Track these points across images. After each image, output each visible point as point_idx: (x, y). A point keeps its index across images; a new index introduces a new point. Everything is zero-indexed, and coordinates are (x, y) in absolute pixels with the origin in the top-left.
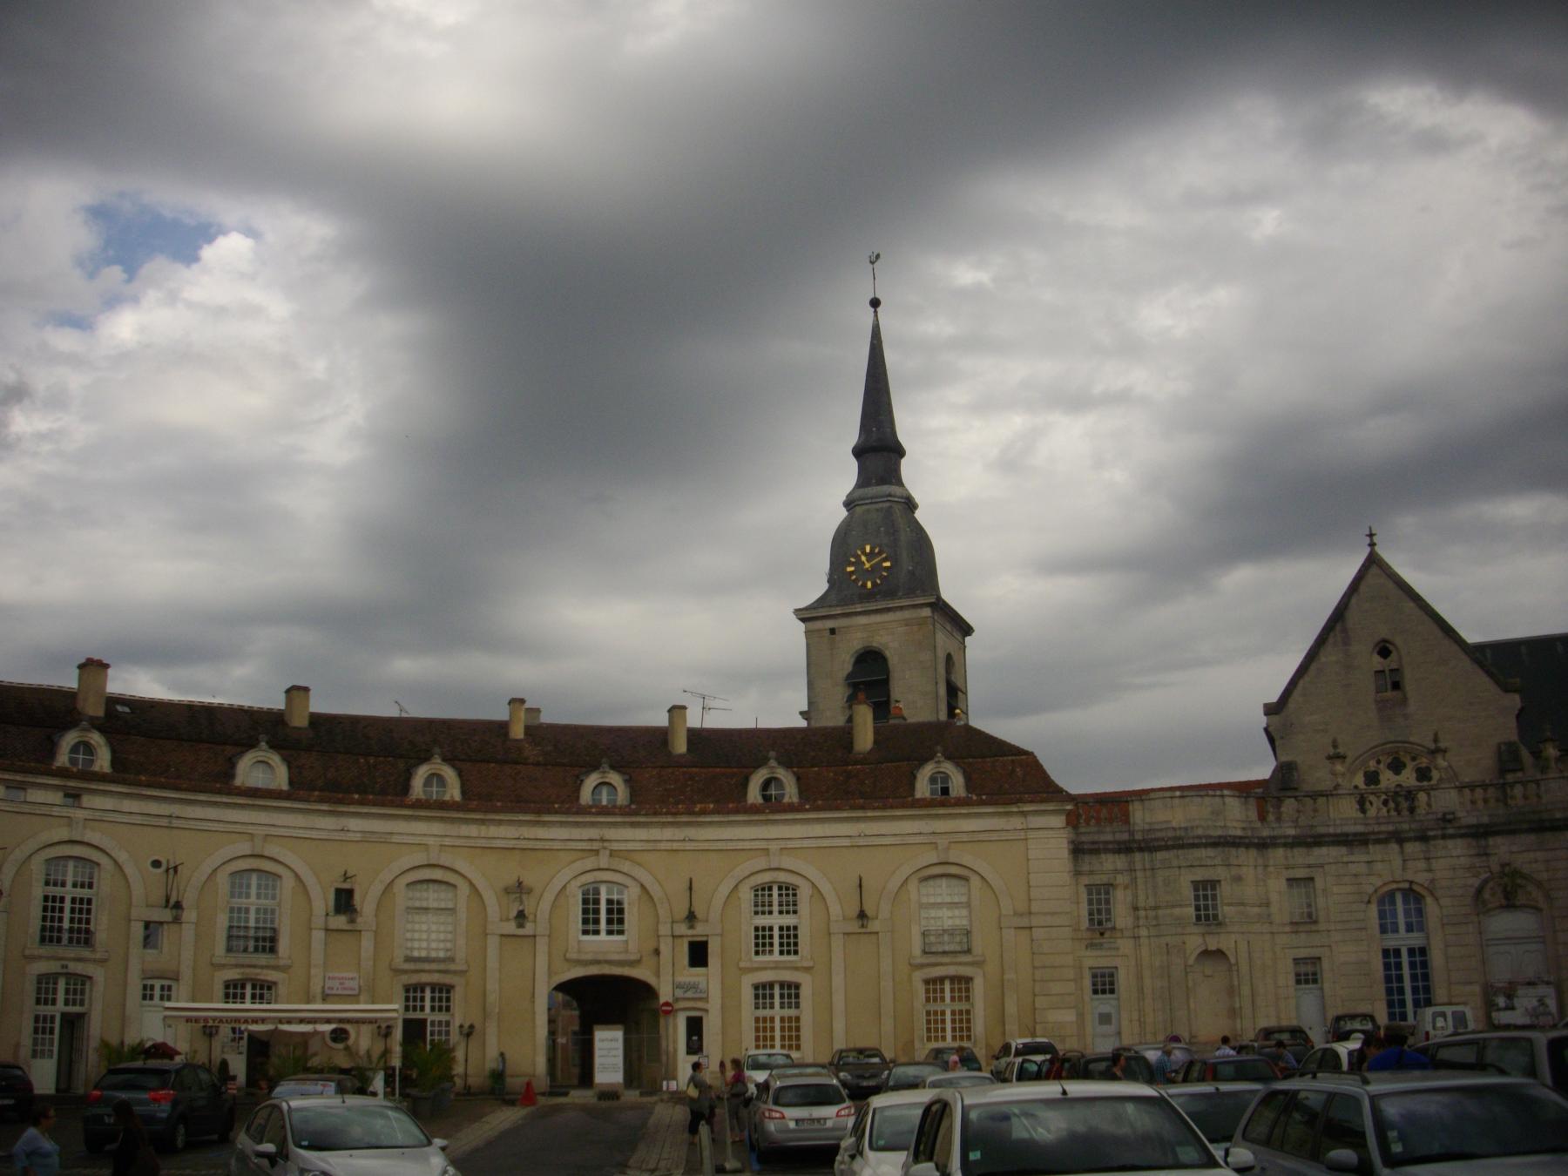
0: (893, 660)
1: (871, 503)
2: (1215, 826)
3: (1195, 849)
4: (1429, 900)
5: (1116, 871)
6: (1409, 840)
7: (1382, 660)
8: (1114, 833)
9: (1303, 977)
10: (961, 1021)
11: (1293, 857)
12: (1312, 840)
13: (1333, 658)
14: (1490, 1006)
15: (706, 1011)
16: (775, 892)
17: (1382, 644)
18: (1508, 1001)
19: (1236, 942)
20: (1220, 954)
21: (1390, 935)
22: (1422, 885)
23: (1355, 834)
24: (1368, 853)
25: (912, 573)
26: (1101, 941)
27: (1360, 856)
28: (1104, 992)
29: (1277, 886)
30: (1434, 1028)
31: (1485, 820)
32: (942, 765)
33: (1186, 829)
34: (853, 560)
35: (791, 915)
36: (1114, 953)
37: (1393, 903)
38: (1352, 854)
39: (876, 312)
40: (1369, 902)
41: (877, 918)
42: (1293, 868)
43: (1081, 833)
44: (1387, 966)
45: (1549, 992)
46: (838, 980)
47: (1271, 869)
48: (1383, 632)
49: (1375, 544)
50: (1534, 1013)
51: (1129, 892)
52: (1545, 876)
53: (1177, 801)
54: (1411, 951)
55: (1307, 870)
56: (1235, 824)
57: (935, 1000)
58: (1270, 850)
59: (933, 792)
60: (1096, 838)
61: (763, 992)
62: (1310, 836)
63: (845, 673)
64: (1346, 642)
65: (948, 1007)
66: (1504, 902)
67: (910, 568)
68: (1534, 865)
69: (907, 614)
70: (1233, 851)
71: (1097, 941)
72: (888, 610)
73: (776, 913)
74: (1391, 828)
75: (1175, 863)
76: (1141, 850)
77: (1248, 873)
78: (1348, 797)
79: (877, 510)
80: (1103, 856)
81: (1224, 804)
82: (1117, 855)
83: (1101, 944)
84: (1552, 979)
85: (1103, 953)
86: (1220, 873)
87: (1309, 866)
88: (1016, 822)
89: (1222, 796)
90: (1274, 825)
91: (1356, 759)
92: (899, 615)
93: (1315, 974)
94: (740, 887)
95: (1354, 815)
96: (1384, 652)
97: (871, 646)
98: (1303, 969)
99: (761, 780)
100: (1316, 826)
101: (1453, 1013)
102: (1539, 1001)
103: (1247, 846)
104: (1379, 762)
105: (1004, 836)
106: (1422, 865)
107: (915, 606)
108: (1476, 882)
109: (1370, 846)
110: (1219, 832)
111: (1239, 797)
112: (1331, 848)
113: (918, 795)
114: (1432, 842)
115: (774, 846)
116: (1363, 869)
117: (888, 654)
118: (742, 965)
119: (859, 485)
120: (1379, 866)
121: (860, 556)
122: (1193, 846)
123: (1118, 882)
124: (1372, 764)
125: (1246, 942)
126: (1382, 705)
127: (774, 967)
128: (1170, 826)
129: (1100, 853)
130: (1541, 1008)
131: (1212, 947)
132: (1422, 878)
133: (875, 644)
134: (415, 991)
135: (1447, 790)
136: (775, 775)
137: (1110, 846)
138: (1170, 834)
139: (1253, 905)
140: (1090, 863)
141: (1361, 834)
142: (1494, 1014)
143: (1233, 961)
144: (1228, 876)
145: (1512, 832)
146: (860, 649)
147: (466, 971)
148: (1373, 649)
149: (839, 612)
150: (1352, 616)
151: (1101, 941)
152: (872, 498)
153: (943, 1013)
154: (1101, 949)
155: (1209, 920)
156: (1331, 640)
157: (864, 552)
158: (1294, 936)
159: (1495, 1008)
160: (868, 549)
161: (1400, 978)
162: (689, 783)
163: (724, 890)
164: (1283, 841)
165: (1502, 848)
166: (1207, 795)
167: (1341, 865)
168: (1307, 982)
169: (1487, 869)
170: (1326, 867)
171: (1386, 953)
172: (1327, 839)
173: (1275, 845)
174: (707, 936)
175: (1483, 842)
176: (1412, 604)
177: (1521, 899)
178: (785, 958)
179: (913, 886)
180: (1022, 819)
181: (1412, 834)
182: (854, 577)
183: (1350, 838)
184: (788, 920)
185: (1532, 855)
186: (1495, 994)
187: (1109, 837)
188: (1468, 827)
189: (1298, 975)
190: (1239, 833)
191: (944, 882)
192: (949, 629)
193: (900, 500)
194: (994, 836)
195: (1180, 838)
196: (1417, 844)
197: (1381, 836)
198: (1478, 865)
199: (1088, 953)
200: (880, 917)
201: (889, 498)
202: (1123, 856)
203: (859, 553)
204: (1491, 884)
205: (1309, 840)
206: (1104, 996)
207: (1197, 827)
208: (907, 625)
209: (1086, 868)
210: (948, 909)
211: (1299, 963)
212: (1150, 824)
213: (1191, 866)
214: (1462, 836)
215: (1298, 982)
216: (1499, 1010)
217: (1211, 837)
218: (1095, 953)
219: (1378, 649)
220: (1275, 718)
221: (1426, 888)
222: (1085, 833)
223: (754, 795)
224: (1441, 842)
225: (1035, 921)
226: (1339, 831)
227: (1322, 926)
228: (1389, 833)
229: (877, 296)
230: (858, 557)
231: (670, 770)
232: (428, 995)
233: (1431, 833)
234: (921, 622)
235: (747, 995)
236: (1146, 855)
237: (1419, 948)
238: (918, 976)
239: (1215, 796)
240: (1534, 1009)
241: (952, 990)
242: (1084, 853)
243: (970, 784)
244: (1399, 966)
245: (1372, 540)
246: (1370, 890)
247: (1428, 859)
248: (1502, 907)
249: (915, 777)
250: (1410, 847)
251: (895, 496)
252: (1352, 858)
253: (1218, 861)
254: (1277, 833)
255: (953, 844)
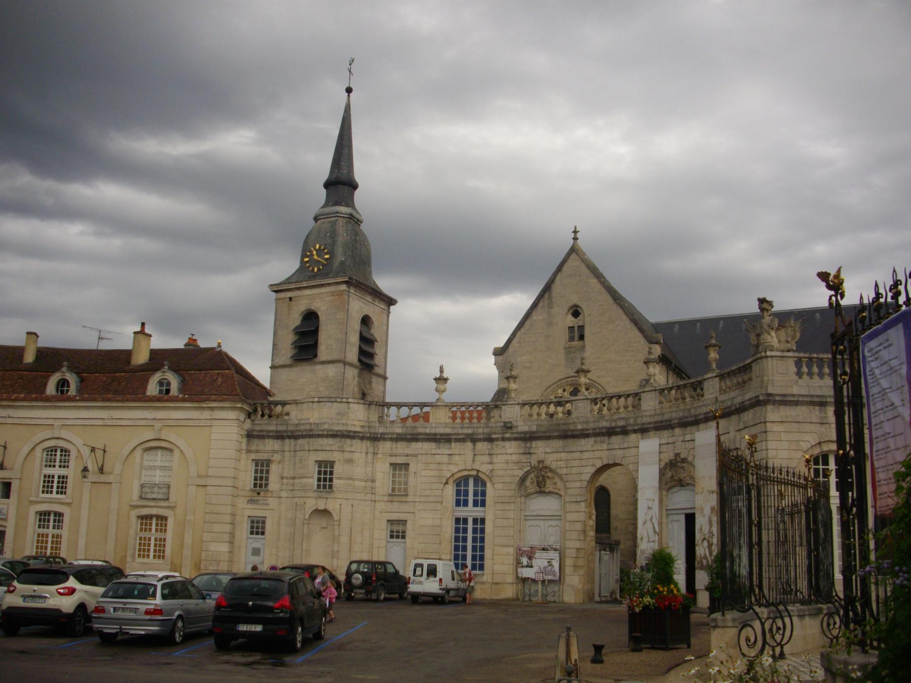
1: (327, 218)
2: (338, 424)
4: (489, 485)
5: (274, 452)
6: (479, 440)
7: (574, 319)
10: (145, 544)
11: (397, 448)
13: (541, 317)
14: (518, 563)
15: (5, 527)
16: (59, 453)
17: (573, 309)
19: (341, 505)
20: (325, 512)
21: (462, 508)
22: (485, 474)
23: (442, 435)
27: (444, 449)
28: (257, 533)
29: (382, 470)
31: (534, 428)
32: (166, 374)
34: (308, 254)
35: (66, 469)
36: (266, 507)
37: (467, 485)
39: (349, 96)
40: (447, 483)
41: (112, 473)
42: (396, 456)
44: (457, 530)
46: (84, 513)
47: (380, 456)
48: (575, 300)
49: (577, 239)
50: (543, 571)
51: (280, 466)
52: (564, 471)
54: (475, 521)
55: (406, 458)
56: (355, 423)
57: (146, 530)
59: (161, 391)
61: (43, 517)
63: (295, 326)
64: (550, 306)
65: (153, 535)
66: (538, 489)
67: (343, 259)
68: (559, 463)
70: (348, 441)
71: (255, 498)
72: (322, 285)
73: (57, 467)
74: (470, 431)
78: (444, 407)
79: (329, 222)
80: (267, 440)
81: (349, 408)
82: (275, 441)
83: (258, 501)
84: (558, 547)
85: (258, 507)
86: (335, 456)
87: (407, 456)
88: (206, 414)
89: (348, 403)
90: (388, 425)
92: (323, 290)
93: (404, 532)
94: (36, 448)
96: (576, 314)
98: (395, 528)
99: (56, 381)
100: (418, 427)
101: (429, 565)
103: (362, 438)
104: (564, 390)
105: (197, 423)
106: (486, 459)
107: (337, 283)
108: (521, 473)
109: (453, 444)
110: (341, 428)
111: (364, 404)
113: (148, 393)
114: (496, 443)
115: (57, 423)
116: (445, 459)
117: (320, 314)
118: (31, 499)
119: (326, 205)
120: (456, 458)
122: (319, 436)
123: (274, 459)
124: (560, 391)
125: (350, 506)
126: (568, 350)
127: (52, 502)
128: (309, 422)
130: (550, 568)
132: (485, 468)
133: (313, 308)
134: (45, 516)
135: (513, 406)
137: (271, 434)
138: (308, 427)
139: (361, 480)
140: (257, 445)
142: (519, 570)
143: (336, 518)
144: (342, 458)
145: (548, 438)
146: (305, 311)
147: (72, 503)
148: (569, 310)
149: (294, 287)
150: (556, 289)
151: (259, 498)
152: (327, 214)
153: (150, 539)
156: (540, 304)
157: (315, 249)
159: (521, 565)
161: (465, 539)
162: (19, 381)
163: (26, 450)
164: (390, 436)
165: (540, 449)
168: (397, 537)
170: (419, 456)
171: (457, 520)
172: (421, 437)
173: (385, 439)
174: (11, 479)
175: (528, 445)
176: (595, 280)
177: (549, 487)
178: (60, 496)
179: (138, 452)
180: (210, 413)
181: (481, 436)
182: (308, 265)
183: (438, 437)
184: (63, 472)
185: (559, 455)
186: (521, 555)
187: (273, 428)
188: (521, 433)
189: (392, 532)
190: (358, 429)
191: (159, 452)
192: (371, 301)
193: (345, 216)
194: (191, 423)
195: (311, 430)
197: (461, 437)
200: (114, 473)
201: (338, 215)
204: (532, 475)
205: (408, 437)
206: (257, 536)
207: (325, 423)
208: (332, 295)
209: (254, 448)
210: (161, 470)
211: (394, 524)
212: (299, 420)
214: (516, 439)
216: (522, 567)
218: (252, 506)
219: (571, 311)
220: (500, 358)
222: (257, 424)
223: (51, 388)
224: (500, 443)
225: (209, 482)
226: (433, 431)
227: (410, 498)
228: (466, 434)
229: (351, 86)
230: (311, 252)
231: (11, 373)
232: (52, 518)
233: (494, 436)
234: (341, 293)
235: (32, 519)
236: (292, 440)
238: (134, 513)
239: (341, 402)
240: (545, 568)
241: (157, 524)
243: (181, 390)
244: (465, 530)
245: (575, 235)
246: (448, 475)
247: (490, 455)
248: (536, 492)
249: (147, 382)
250: (480, 446)
251: (341, 213)
252: (438, 451)
254: (388, 431)
255: (165, 427)
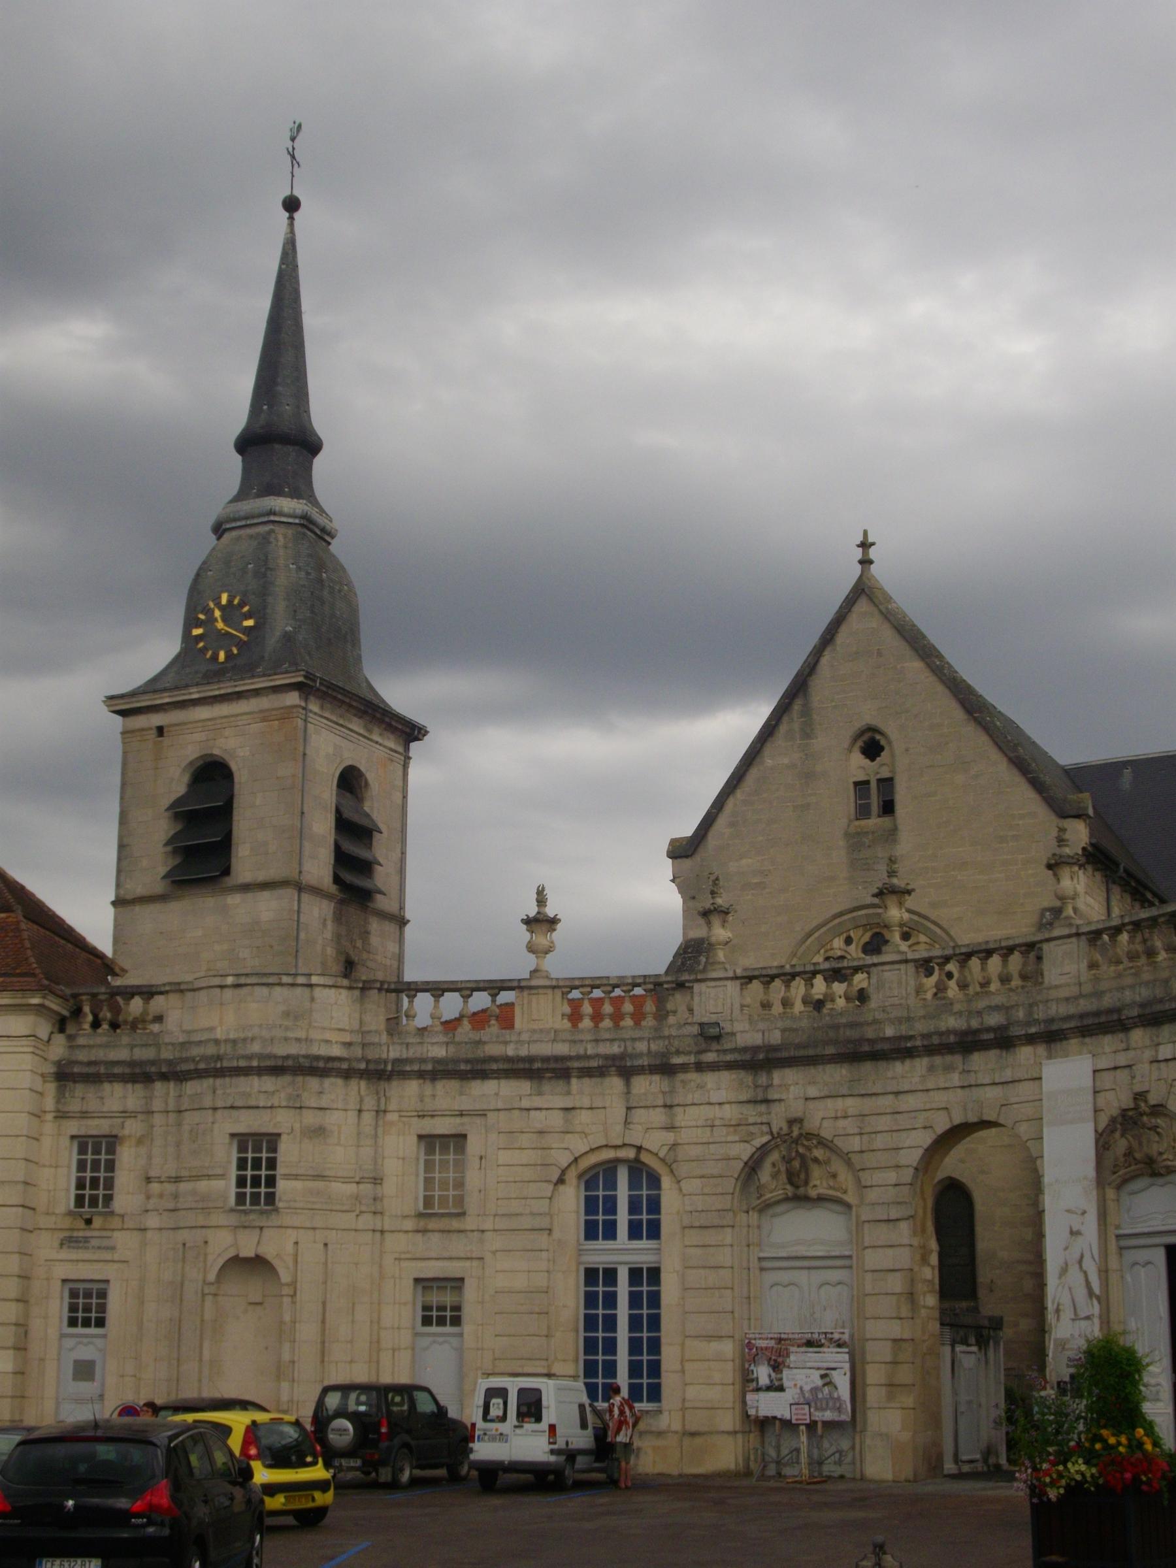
0: (241, 776)
2: (286, 1039)
3: (242, 1079)
4: (666, 1182)
5: (126, 1114)
6: (640, 1070)
8: (132, 1047)
9: (434, 1313)
11: (434, 1096)
12: (469, 1067)
17: (866, 737)
18: (773, 1375)
20: (258, 1264)
21: (601, 1244)
24: (569, 1093)
25: (288, 638)
26: (88, 1234)
27: (553, 1096)
28: (86, 1323)
30: (486, 1417)
31: (776, 1038)
33: (234, 1042)
34: (202, 617)
36: (107, 1256)
37: (612, 1184)
38: (540, 1094)
39: (291, 218)
40: (561, 1181)
42: (433, 1116)
43: (79, 1046)
44: (590, 1300)
45: (838, 1358)
47: (392, 1117)
48: (868, 715)
50: (810, 1400)
51: (143, 1150)
52: (855, 1143)
53: (228, 994)
54: (635, 1274)
55: (458, 1120)
56: (328, 1036)
58: (395, 1083)
60: (100, 1054)
62: (467, 1061)
64: (807, 733)
67: (289, 628)
68: (841, 1123)
69: (264, 702)
70: (313, 1083)
71: (81, 1234)
72: (239, 696)
74: (615, 1049)
75: (207, 1102)
76: (164, 1077)
77: (341, 1122)
78: (550, 991)
79: (251, 537)
81: (312, 999)
82: (129, 1086)
83: (86, 1239)
84: (846, 1337)
85: (87, 1255)
86: (281, 1121)
89: (310, 986)
91: (809, 935)
93: (457, 1308)
95: (558, 1026)
96: (872, 748)
97: (212, 755)
98: (435, 1298)
100: (485, 1043)
102: (823, 1377)
103: (347, 1075)
104: (849, 941)
106: (658, 1117)
107: (276, 689)
108: (745, 1151)
109: (574, 1081)
112: (503, 1082)
114: (681, 1076)
116: (556, 1120)
121: (213, 611)
122: (245, 1072)
123: (126, 1132)
124: (838, 943)
126: (855, 841)
128: (212, 1036)
129: (101, 1082)
130: (826, 1390)
131: (248, 1252)
132: (656, 1141)
133: (216, 752)
136: (842, 994)
138: (211, 1050)
139: (347, 1180)
141: (557, 1059)
143: (285, 1277)
144: (297, 1126)
149: (167, 700)
150: (822, 688)
151: (88, 1234)
152: (246, 518)
154: (87, 1248)
155: (258, 1204)
157: (218, 604)
158: (419, 1236)
160: (224, 599)
164: (416, 1067)
166: (280, 984)
167: (517, 1112)
168: (441, 1321)
169: (765, 1128)
170: (490, 1114)
171: (591, 1275)
172: (494, 1066)
173: (404, 1075)
175: (763, 1079)
176: (918, 665)
177: (819, 1184)
181: (645, 1061)
182: (201, 645)
183: (537, 1065)
186: (754, 1360)
187: (123, 1054)
188: (745, 1050)
189: (426, 1308)
190: (336, 1051)
193: (290, 520)
196: (656, 1078)
197: (594, 1063)
198: (751, 1120)
199: (65, 1254)
201: (272, 518)
202: (138, 1086)
203: (212, 605)
204: (775, 1156)
205: (463, 1067)
207: (253, 1039)
208: (264, 720)
209: (74, 1106)
212: (189, 1032)
213: (232, 1107)
214: (730, 1066)
215: (427, 1321)
216: (758, 1389)
217: (275, 1057)
219: (860, 743)
220: (687, 863)
221: (663, 1160)
224: (693, 1076)
228: (606, 1057)
229: (296, 193)
230: (209, 612)
233: (677, 1060)
234: (286, 714)
237: (649, 1269)
239: (293, 985)
242: (75, 1082)
246: (564, 1159)
248: (787, 1199)
250: (644, 1085)
251: (281, 514)
252: (537, 1102)
253: (280, 1099)
